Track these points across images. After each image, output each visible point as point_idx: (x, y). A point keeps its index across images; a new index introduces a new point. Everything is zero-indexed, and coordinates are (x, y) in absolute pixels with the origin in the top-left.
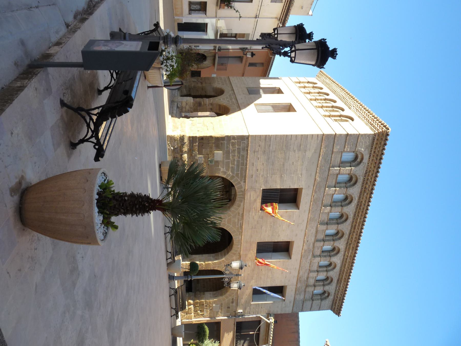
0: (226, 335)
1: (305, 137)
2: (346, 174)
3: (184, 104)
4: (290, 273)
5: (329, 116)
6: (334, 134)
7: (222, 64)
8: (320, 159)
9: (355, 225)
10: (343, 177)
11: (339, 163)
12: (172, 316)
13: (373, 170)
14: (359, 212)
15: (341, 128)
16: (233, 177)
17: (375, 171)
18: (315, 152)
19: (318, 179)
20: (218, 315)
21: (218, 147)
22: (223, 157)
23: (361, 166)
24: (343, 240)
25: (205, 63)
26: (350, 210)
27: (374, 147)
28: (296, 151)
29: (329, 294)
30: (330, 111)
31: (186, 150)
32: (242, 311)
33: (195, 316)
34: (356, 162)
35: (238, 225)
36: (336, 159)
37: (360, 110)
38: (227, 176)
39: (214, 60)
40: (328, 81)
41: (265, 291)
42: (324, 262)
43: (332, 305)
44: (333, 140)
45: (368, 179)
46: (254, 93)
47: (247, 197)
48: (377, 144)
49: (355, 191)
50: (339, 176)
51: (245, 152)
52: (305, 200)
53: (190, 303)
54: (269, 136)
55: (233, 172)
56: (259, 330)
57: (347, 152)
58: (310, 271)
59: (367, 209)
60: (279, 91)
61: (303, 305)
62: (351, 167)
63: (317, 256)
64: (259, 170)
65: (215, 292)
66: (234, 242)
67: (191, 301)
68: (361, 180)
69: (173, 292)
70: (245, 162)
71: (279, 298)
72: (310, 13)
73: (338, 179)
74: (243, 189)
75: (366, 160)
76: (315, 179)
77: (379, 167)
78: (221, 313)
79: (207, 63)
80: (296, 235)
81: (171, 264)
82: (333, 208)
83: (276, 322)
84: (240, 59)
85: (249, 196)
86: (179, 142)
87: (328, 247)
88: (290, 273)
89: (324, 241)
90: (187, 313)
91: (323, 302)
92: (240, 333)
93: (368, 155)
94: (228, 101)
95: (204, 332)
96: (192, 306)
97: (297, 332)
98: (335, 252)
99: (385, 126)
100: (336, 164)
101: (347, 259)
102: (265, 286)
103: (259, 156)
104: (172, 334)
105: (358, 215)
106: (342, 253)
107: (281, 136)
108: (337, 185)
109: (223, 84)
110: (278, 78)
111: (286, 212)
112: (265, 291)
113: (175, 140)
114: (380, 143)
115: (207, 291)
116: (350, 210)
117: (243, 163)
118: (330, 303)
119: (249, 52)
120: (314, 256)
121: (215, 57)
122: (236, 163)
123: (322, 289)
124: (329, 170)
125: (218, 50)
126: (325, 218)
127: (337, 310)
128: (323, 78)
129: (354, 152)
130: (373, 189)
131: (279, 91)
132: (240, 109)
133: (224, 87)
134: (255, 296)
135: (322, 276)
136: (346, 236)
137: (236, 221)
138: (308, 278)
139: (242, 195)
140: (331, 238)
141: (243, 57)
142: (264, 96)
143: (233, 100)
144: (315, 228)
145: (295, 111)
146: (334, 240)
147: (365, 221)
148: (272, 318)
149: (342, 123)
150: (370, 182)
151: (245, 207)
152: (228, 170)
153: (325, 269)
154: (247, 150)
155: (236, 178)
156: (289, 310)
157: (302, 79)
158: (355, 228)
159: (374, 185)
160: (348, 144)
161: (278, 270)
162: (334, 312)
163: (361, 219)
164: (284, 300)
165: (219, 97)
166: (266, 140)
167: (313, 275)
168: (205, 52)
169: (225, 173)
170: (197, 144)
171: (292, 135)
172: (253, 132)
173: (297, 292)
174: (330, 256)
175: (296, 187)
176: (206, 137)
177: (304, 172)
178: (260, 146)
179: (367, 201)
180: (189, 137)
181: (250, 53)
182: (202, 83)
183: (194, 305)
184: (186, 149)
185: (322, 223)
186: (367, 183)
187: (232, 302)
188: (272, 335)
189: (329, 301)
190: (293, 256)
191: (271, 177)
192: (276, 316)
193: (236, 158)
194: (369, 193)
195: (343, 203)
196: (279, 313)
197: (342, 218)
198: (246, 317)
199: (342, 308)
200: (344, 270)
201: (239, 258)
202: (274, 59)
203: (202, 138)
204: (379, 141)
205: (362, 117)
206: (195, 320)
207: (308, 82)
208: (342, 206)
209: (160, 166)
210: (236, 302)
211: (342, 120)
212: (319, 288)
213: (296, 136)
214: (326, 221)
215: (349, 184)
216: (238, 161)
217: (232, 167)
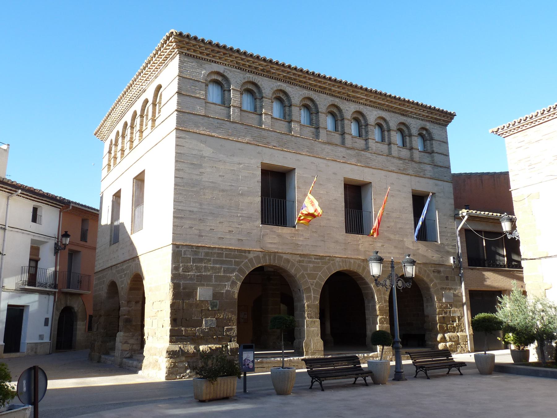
0: (488, 283)
1: (180, 158)
2: (241, 97)
3: (126, 347)
4: (392, 184)
5: (154, 121)
6: (176, 112)
7: (80, 282)
8: (216, 135)
9: (320, 87)
10: (247, 102)
11: (223, 108)
12: (461, 374)
13: (236, 57)
14: (300, 81)
15: (170, 104)
16: (241, 271)
17: (236, 55)
18: (205, 142)
19: (247, 139)
20: (459, 294)
21: (191, 294)
22: (207, 285)
23: (228, 75)
24: (342, 106)
25: (76, 309)
26: (297, 94)
27: (199, 55)
28: (201, 170)
29: (423, 128)
30: (147, 119)
31: (192, 347)
32: (452, 258)
33: (462, 331)
34: (224, 83)
35: (319, 263)
36: (218, 111)
37: (147, 76)
38: (239, 280)
39: (72, 294)
40: (108, 124)
41: (420, 223)
42: (376, 134)
43: (439, 124)
44: (186, 114)
45: (249, 66)
46: (117, 233)
47: (273, 248)
48: (195, 51)
49: (268, 86)
50: (245, 108)
51: (201, 250)
52: (279, 159)
53: (441, 338)
54: (174, 213)
55: (233, 271)
56: (479, 232)
57: (206, 96)
58: (389, 154)
59: (295, 69)
60: (117, 195)
61: (441, 167)
62: (230, 90)
63: (367, 144)
64: (231, 229)
65: (425, 299)
66: (345, 269)
67: (439, 337)
68: (251, 76)
69: (422, 373)
70: (216, 251)
71: (430, 201)
72: (5, 147)
73: (249, 110)
74: (261, 255)
75: (220, 68)
76: (247, 143)
77: (231, 49)
78: (455, 290)
79: (76, 305)
80: (335, 174)
81: (373, 378)
82: (294, 118)
83: (467, 207)
84: (73, 254)
85: (273, 246)
86: (178, 360)
87: (353, 128)
88: (392, 184)
89: (343, 134)
90: (458, 343)
91: (436, 137)
92: (485, 260)
93: (213, 64)
94: (125, 275)
95: (484, 320)
96: (447, 335)
97: (476, 174)
98: (361, 118)
99: (168, 38)
100: (225, 112)
101: (371, 101)
102: (413, 222)
103: (208, 229)
104: (490, 373)
105: (305, 82)
106: (362, 108)
107: (175, 194)
108: (258, 112)
109: (104, 281)
110: (102, 198)
111: (299, 188)
112: (420, 223)
113: (175, 365)
114: (194, 45)
115: (423, 310)
116: (297, 94)
117: (218, 253)
118: (437, 127)
119: (61, 239)
120: (367, 149)
121: (66, 294)
122: (218, 266)
123: (416, 138)
124: (233, 122)
125: (55, 287)
126: (309, 132)
127: (447, 117)
128: (104, 130)
129: (207, 85)
130: (265, 60)
131: (117, 195)
132: (137, 257)
133: (107, 281)
134: (428, 239)
135: (397, 138)
136: (337, 101)
137: (311, 265)
138: (400, 159)
139: (270, 256)
140: (339, 122)
141: (70, 250)
142: (121, 220)
143: (124, 267)
144: (324, 146)
145: (144, 171)
146: (343, 119)
147: (313, 73)
148: (460, 212)
149: (163, 102)
150: (253, 63)
151: (290, 251)
152: (230, 277)
153: (386, 133)
154: (198, 247)
155: (241, 265)
156: (448, 188)
157: (105, 161)
158: (325, 88)
159: (258, 57)
160: (193, 92)
161: (388, 202)
162: (450, 122)
163: (310, 79)
164: (433, 194)
165: (120, 289)
166: (182, 218)
167: (395, 150)
168: (57, 309)
169: (234, 284)
170: (183, 329)
171: (175, 177)
172: (168, 238)
173: (422, 174)
174: (367, 125)
175: (259, 173)
176: (171, 313)
177: (236, 159)
178: (191, 228)
179: (282, 68)
180: (171, 341)
181: (64, 239)
182: (100, 316)
183: (444, 332)
184: (191, 348)
185: (317, 136)
186: (256, 68)
187: (439, 272)
188: (487, 213)
189: (435, 130)
190: (367, 179)
191: (242, 210)
192: (458, 206)
193: (210, 265)
194: (270, 64)
195: (287, 103)
196: (452, 201)
197: (310, 106)
198: (460, 251)
199: (443, 110)
200: (388, 106)
201: (366, 262)
202: (75, 203)
203: (174, 321)
204: (189, 46)
205: (157, 73)
206: (468, 331)
207: (110, 152)
208: (290, 106)
209: (202, 402)
210: (438, 267)
211: (160, 103)
212: (414, 142)
213: (177, 170)
214: (313, 130)
215: (257, 94)
216: (215, 262)
217: (224, 271)
